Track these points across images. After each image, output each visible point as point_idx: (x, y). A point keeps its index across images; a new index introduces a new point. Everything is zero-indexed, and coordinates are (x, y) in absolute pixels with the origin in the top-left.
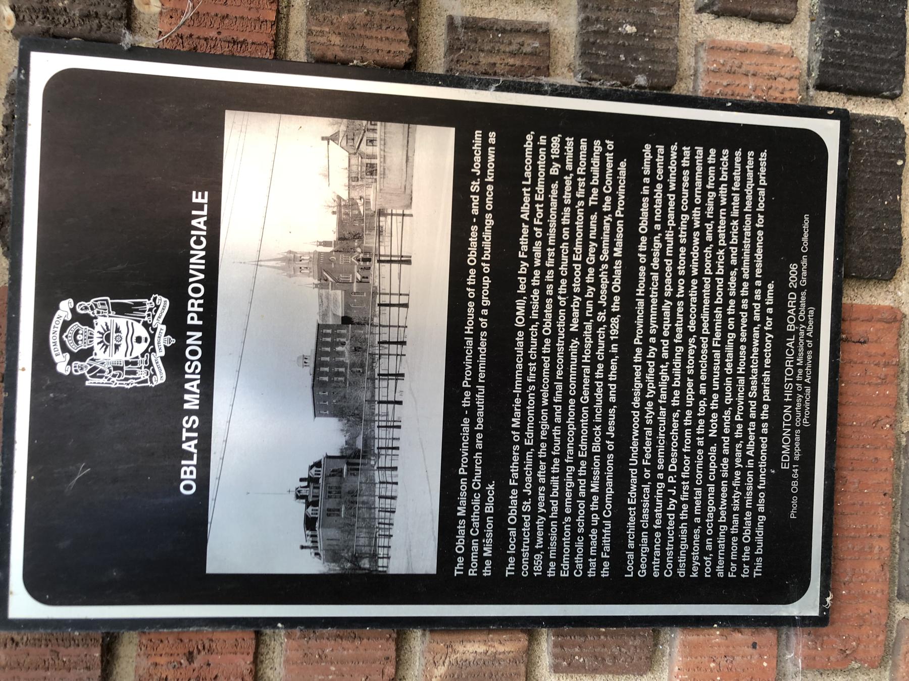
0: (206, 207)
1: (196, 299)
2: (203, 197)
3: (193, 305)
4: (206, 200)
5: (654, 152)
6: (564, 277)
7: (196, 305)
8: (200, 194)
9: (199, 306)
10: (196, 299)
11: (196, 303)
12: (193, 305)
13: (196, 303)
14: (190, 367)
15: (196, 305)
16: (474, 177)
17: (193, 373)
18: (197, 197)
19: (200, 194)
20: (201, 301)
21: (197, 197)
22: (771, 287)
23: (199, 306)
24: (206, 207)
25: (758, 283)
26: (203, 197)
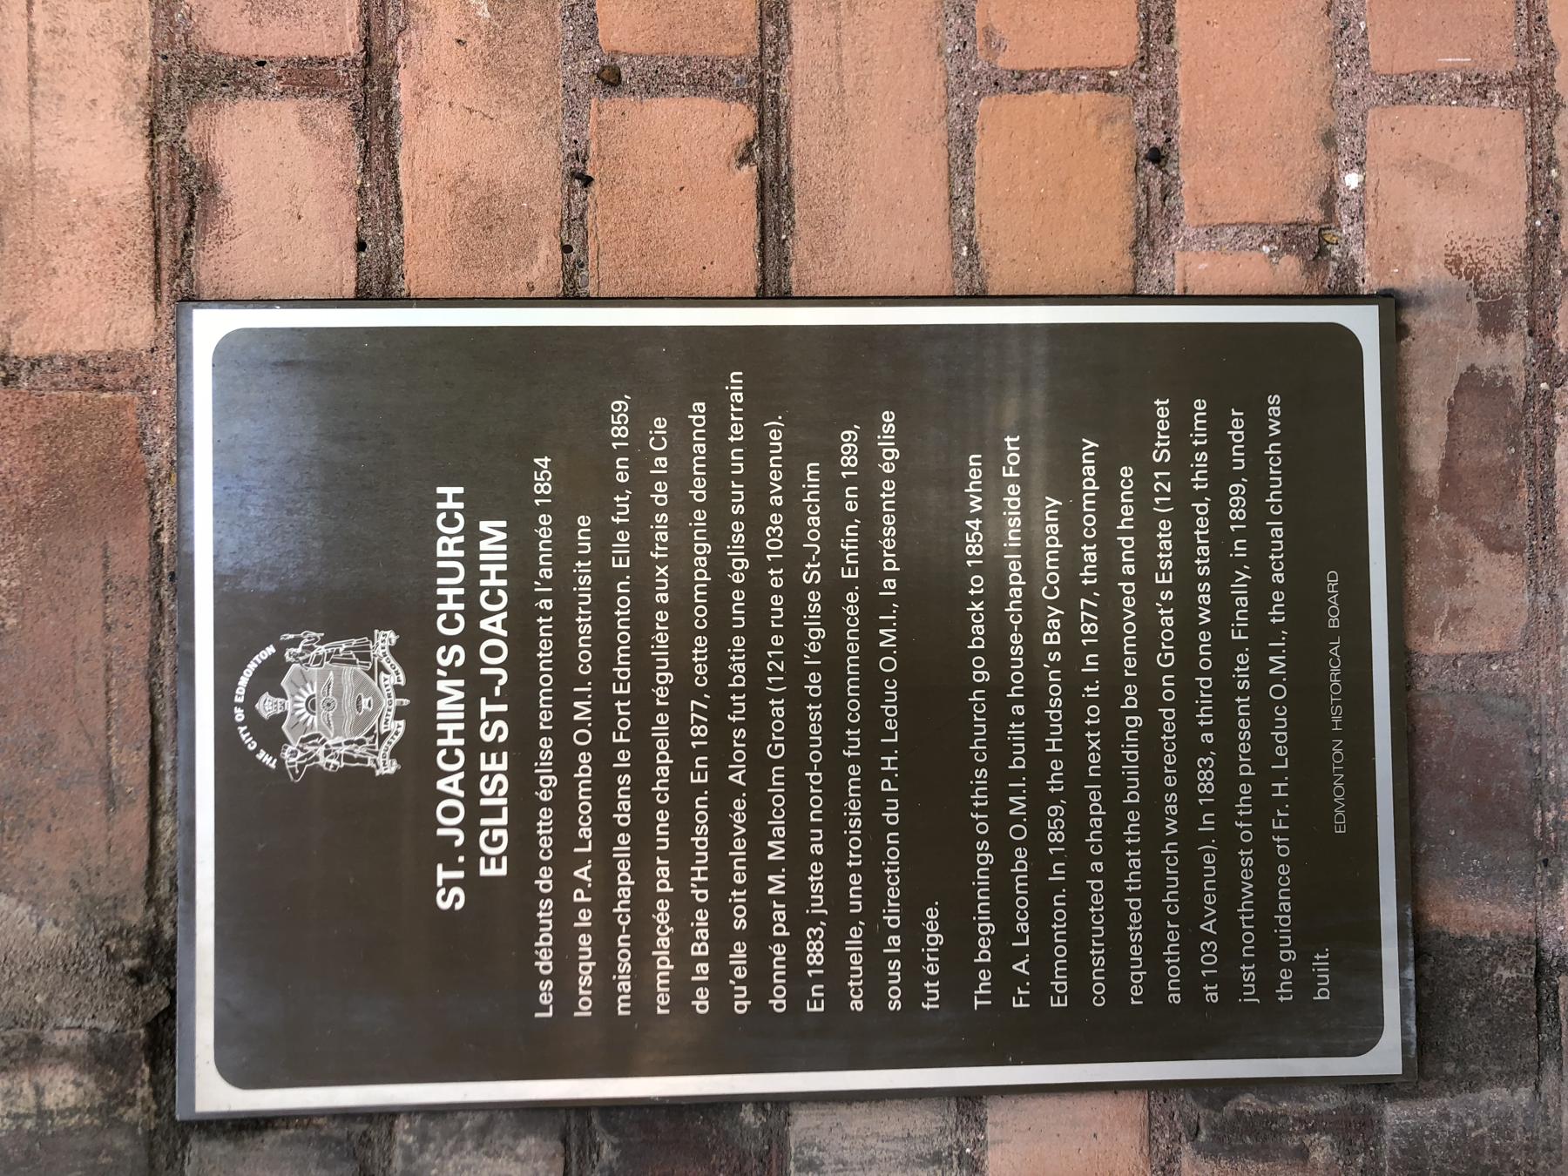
0: (505, 811)
1: (451, 536)
2: (499, 761)
3: (445, 547)
4: (504, 766)
5: (913, 993)
6: (546, 864)
7: (451, 547)
8: (493, 756)
9: (457, 547)
10: (451, 536)
11: (451, 542)
12: (445, 547)
13: (451, 542)
14: (488, 785)
15: (451, 547)
16: (446, 852)
17: (495, 795)
18: (488, 761)
19: (493, 756)
20: (461, 539)
21: (488, 761)
22: (1321, 960)
23: (457, 547)
24: (505, 811)
25: (1288, 954)
26: (499, 761)
